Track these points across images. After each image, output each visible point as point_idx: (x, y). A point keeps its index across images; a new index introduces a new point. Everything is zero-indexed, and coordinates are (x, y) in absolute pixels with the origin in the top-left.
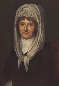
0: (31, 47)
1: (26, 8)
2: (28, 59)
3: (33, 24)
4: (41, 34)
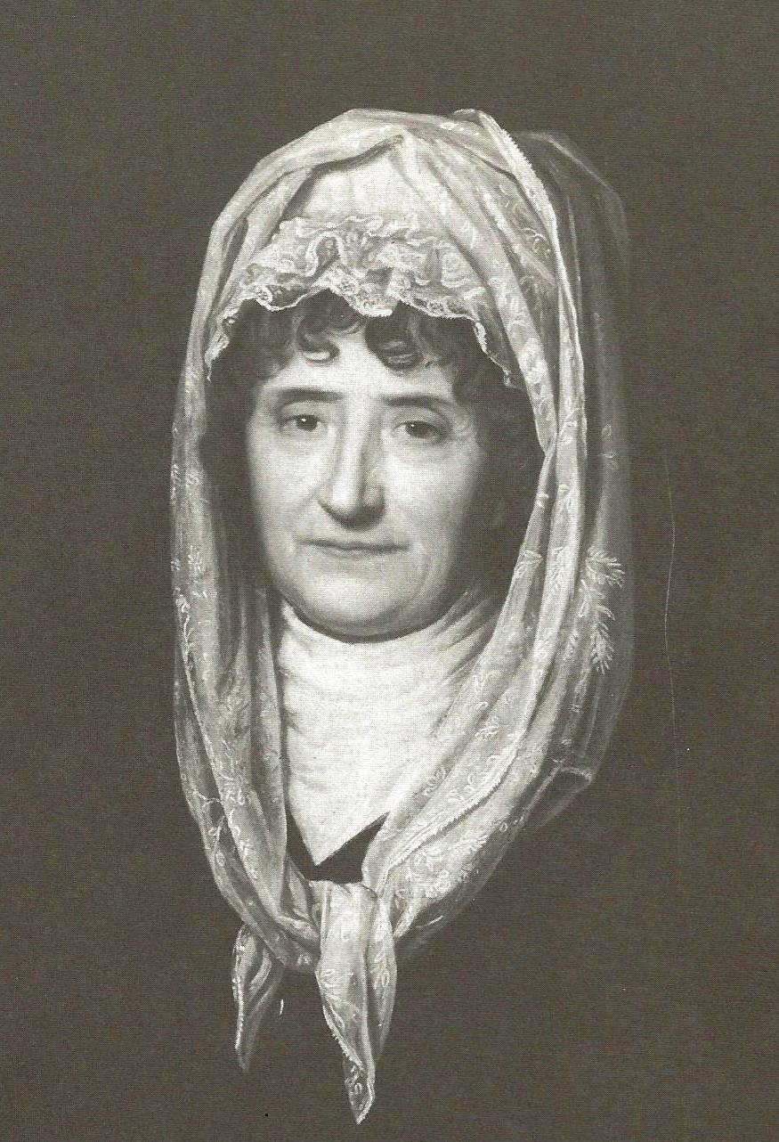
0: (437, 753)
1: (359, 175)
2: (383, 933)
3: (452, 415)
4: (583, 554)
